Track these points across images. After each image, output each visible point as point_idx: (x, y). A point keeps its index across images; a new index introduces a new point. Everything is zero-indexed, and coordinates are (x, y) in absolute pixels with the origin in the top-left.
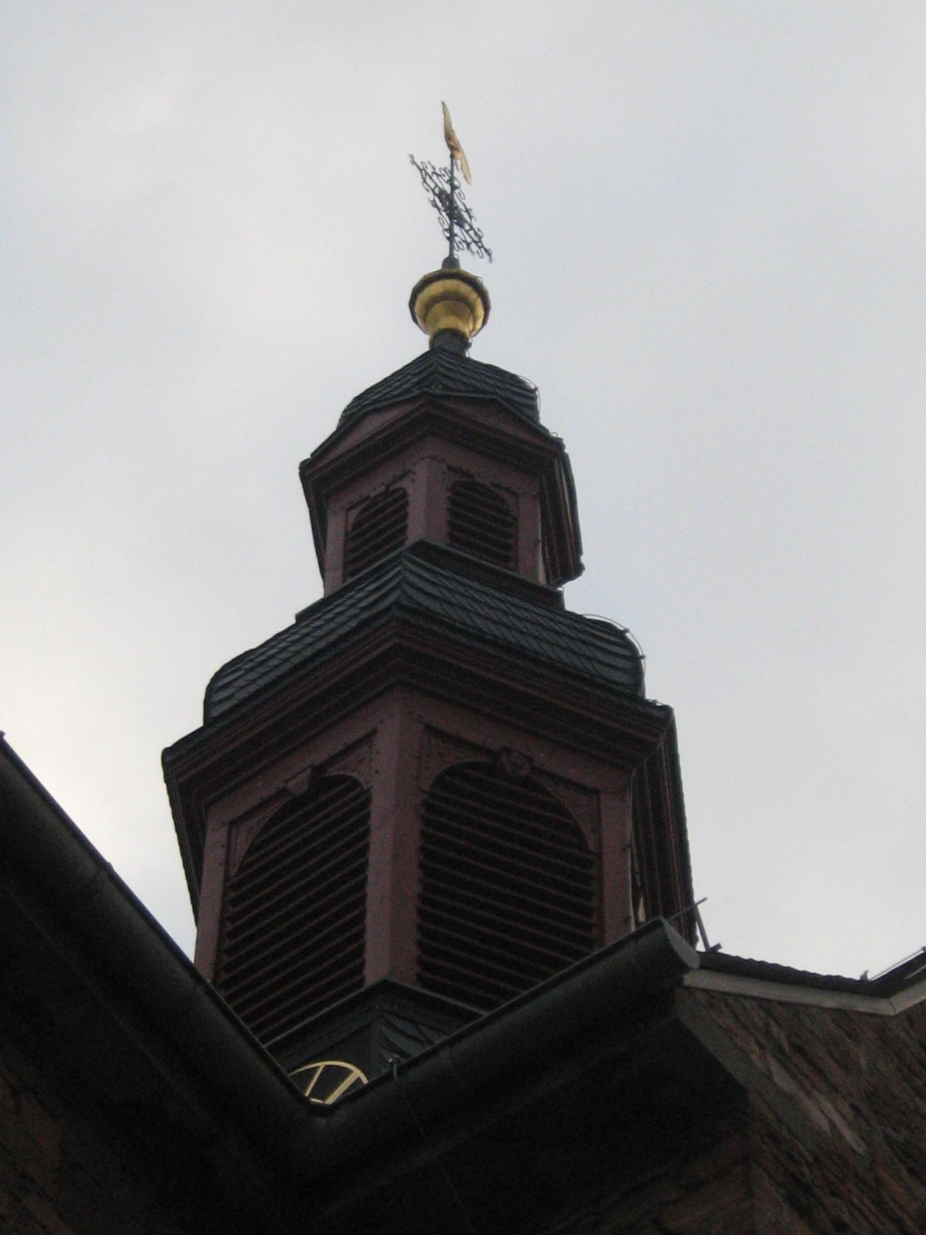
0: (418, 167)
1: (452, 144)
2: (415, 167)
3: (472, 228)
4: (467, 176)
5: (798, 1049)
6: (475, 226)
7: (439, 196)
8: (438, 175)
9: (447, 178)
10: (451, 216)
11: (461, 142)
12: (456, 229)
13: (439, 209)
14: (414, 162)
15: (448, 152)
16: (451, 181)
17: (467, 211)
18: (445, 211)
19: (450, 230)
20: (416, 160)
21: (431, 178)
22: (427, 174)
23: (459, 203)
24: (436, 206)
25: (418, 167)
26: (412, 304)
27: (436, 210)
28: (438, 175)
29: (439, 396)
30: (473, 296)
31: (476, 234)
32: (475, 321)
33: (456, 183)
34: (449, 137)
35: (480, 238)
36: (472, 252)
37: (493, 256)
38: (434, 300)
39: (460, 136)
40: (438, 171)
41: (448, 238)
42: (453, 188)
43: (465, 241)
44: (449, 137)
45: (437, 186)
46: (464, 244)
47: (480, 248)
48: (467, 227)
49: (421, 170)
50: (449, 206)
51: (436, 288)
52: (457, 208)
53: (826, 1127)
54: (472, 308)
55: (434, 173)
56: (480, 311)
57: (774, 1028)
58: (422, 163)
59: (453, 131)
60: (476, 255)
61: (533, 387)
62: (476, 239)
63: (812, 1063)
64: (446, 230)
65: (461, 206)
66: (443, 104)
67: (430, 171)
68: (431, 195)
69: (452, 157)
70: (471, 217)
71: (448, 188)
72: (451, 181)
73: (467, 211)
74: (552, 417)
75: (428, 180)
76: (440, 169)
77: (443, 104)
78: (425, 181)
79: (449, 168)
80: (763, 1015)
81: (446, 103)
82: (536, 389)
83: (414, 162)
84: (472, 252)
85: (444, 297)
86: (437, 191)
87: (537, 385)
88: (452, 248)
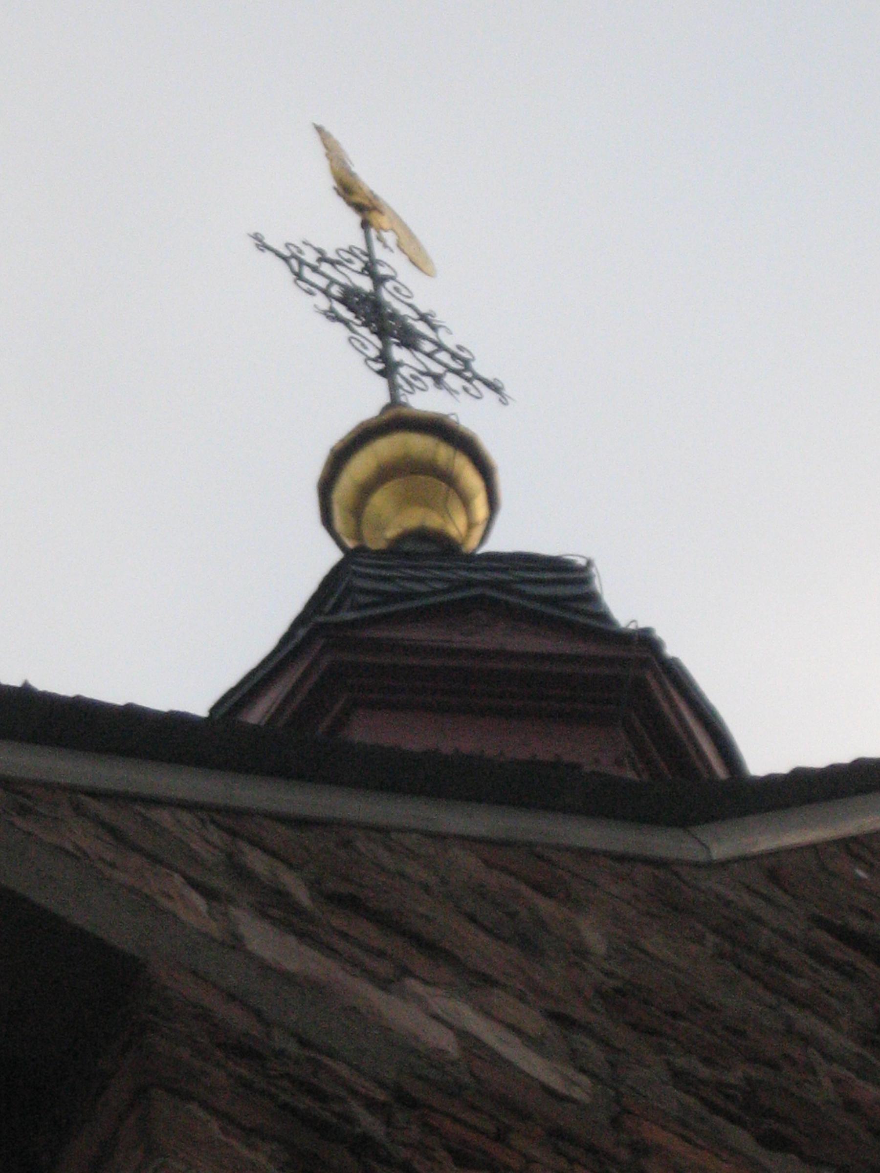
0: (278, 254)
1: (357, 199)
2: (268, 255)
3: (440, 347)
4: (416, 258)
5: (352, 904)
6: (449, 342)
7: (343, 301)
8: (333, 263)
9: (358, 265)
10: (382, 333)
11: (378, 192)
12: (398, 353)
13: (346, 323)
14: (263, 246)
15: (354, 219)
16: (369, 269)
17: (423, 318)
18: (365, 324)
19: (384, 357)
20: (268, 241)
21: (315, 269)
22: (302, 263)
23: (397, 306)
24: (336, 318)
25: (278, 254)
26: (327, 520)
27: (339, 327)
28: (333, 263)
29: (353, 624)
30: (443, 453)
31: (454, 356)
32: (466, 503)
33: (382, 271)
34: (348, 189)
35: (466, 363)
36: (451, 391)
37: (507, 391)
38: (366, 490)
39: (371, 179)
40: (331, 255)
41: (381, 373)
42: (379, 281)
43: (428, 374)
44: (348, 189)
45: (333, 282)
46: (428, 381)
47: (468, 380)
48: (428, 347)
49: (285, 259)
50: (372, 313)
51: (361, 466)
52: (394, 316)
53: (447, 1042)
54: (449, 479)
55: (323, 259)
56: (471, 479)
57: (257, 861)
58: (287, 245)
59: (353, 175)
60: (463, 396)
61: (582, 562)
62: (454, 365)
63: (384, 920)
64: (375, 360)
65: (404, 310)
66: (319, 129)
67: (310, 257)
68: (323, 302)
69: (365, 225)
70: (434, 328)
71: (365, 284)
72: (369, 269)
73: (423, 318)
74: (626, 603)
75: (307, 273)
76: (337, 252)
77: (319, 129)
78: (299, 276)
79: (362, 246)
80: (215, 835)
81: (328, 128)
82: (589, 563)
83: (263, 246)
84: (451, 391)
85: (384, 474)
86: (335, 290)
87: (588, 555)
88: (393, 388)
